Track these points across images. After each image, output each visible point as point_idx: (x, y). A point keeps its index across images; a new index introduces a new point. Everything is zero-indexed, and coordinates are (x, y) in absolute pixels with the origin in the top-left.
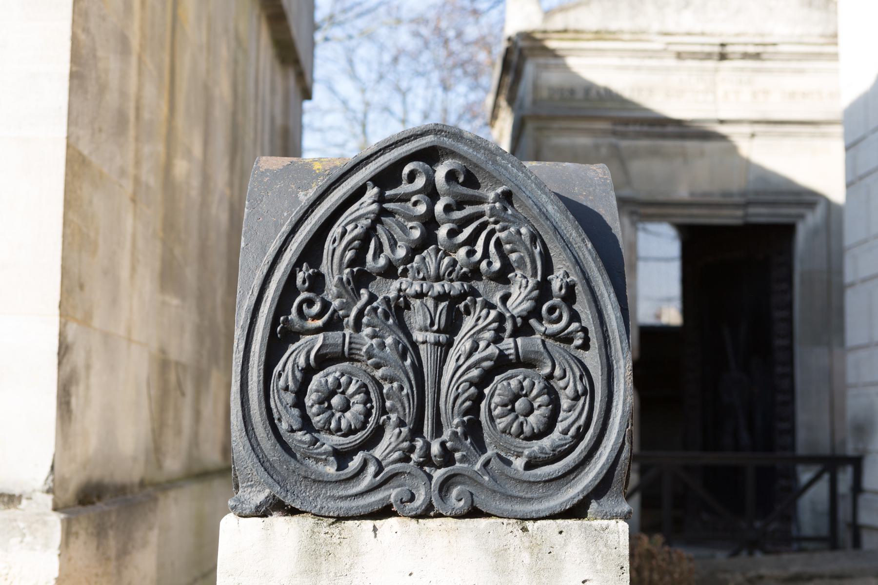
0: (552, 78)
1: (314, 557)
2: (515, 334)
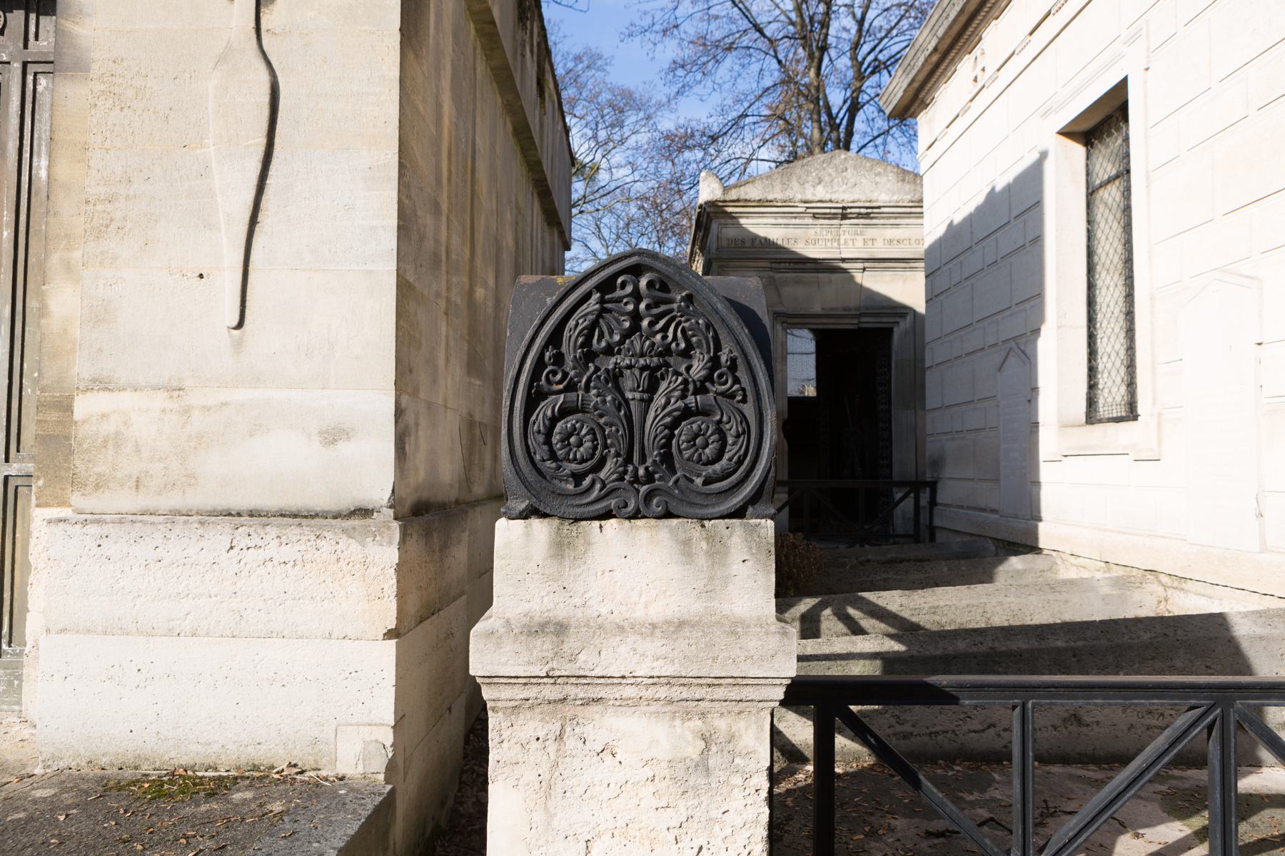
0: (730, 232)
1: (560, 548)
2: (695, 393)
